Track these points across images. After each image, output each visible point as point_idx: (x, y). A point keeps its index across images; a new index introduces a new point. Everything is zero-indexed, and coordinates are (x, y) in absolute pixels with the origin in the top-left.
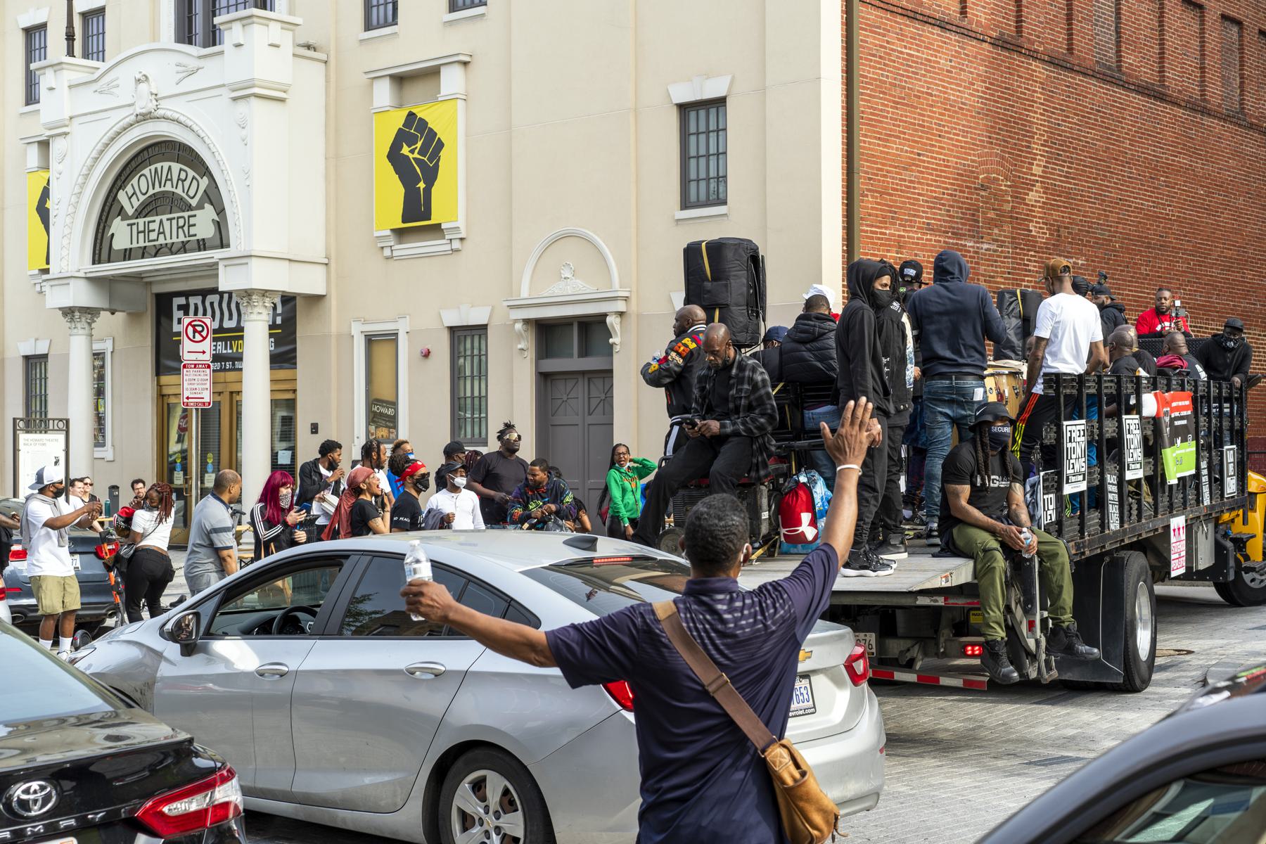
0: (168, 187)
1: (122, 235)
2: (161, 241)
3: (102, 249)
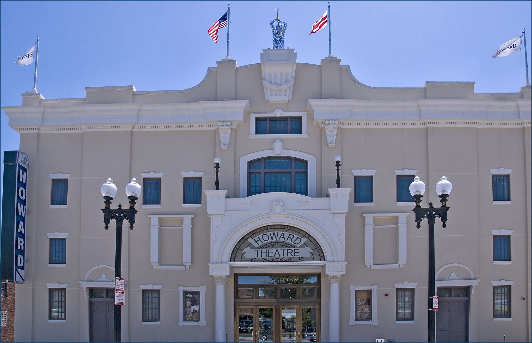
0: (282, 240)
1: (249, 252)
2: (277, 256)
3: (236, 254)
